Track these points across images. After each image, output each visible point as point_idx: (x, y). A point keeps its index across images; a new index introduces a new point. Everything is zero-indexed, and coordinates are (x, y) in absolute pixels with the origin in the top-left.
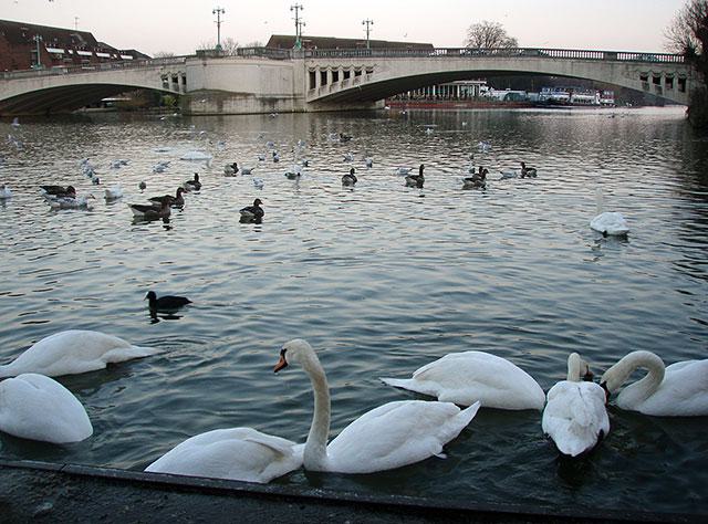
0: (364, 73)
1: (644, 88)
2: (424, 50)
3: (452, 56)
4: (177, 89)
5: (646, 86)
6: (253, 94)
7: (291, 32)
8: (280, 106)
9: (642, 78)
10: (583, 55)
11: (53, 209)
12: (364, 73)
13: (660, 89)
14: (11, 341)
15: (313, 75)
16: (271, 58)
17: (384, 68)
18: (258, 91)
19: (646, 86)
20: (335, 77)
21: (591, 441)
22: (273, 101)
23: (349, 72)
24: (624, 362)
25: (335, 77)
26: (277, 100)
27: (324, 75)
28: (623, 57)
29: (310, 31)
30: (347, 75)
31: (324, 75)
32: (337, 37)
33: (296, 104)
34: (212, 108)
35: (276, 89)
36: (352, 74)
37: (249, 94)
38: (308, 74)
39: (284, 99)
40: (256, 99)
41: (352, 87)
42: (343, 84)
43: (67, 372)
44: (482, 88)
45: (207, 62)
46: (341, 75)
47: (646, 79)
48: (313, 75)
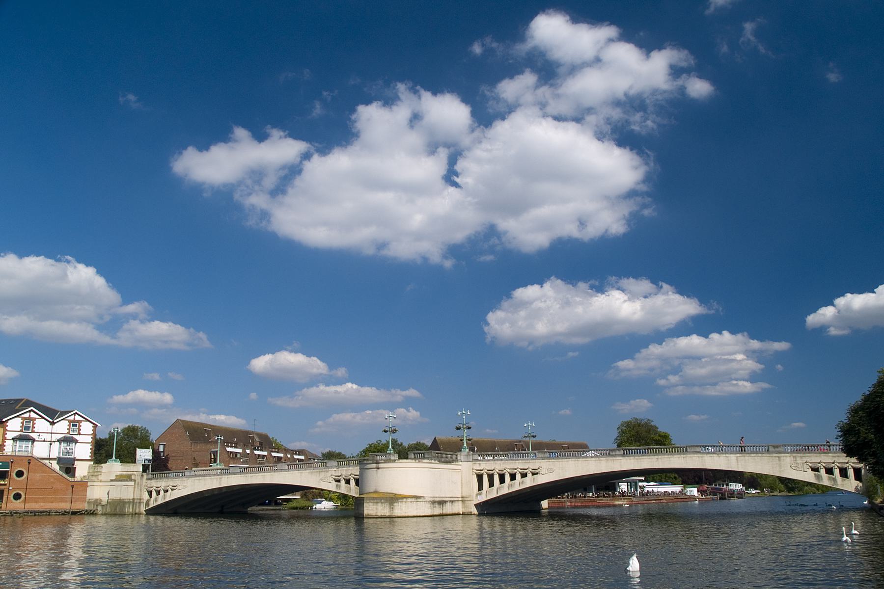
5: (819, 477)
6: (424, 497)
8: (448, 509)
9: (813, 469)
11: (523, 551)
15: (480, 478)
16: (440, 462)
17: (551, 471)
18: (428, 493)
19: (819, 477)
20: (502, 480)
21: (846, 295)
22: (442, 503)
24: (843, 317)
25: (502, 480)
26: (445, 502)
27: (491, 478)
31: (491, 478)
33: (464, 506)
35: (444, 493)
37: (420, 497)
38: (475, 477)
39: (452, 502)
41: (152, 506)
42: (510, 486)
44: (641, 484)
45: (381, 465)
46: (496, 479)
47: (339, 481)
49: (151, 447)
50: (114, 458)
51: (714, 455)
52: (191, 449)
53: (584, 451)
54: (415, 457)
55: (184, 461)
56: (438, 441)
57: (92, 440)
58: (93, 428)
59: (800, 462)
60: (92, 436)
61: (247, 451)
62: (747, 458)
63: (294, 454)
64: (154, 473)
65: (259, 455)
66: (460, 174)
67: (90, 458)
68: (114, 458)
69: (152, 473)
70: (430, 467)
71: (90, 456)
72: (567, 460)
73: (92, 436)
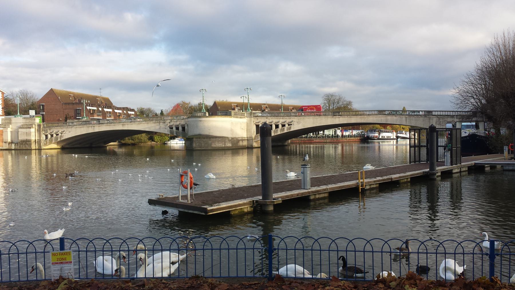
49: (506, 148)
50: (19, 114)
51: (393, 116)
52: (63, 108)
53: (348, 112)
54: (221, 114)
55: (58, 115)
56: (217, 104)
57: (2, 102)
58: (1, 95)
59: (442, 120)
60: (2, 100)
61: (99, 108)
62: (412, 118)
63: (115, 109)
64: (285, 112)
65: (107, 112)
66: (161, 110)
67: (2, 114)
68: (19, 114)
69: (284, 112)
70: (457, 140)
71: (2, 113)
72: (300, 117)
73: (2, 100)
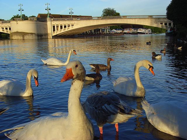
0: (71, 26)
1: (166, 28)
2: (89, 18)
3: (99, 19)
4: (7, 32)
7: (46, 12)
10: (161, 17)
12: (71, 26)
13: (167, 27)
14: (15, 118)
15: (54, 27)
17: (77, 24)
23: (66, 26)
26: (43, 35)
28: (154, 17)
29: (53, 12)
30: (65, 27)
32: (168, 5)
34: (20, 38)
36: (67, 26)
40: (36, 35)
43: (157, 128)
48: (54, 27)
